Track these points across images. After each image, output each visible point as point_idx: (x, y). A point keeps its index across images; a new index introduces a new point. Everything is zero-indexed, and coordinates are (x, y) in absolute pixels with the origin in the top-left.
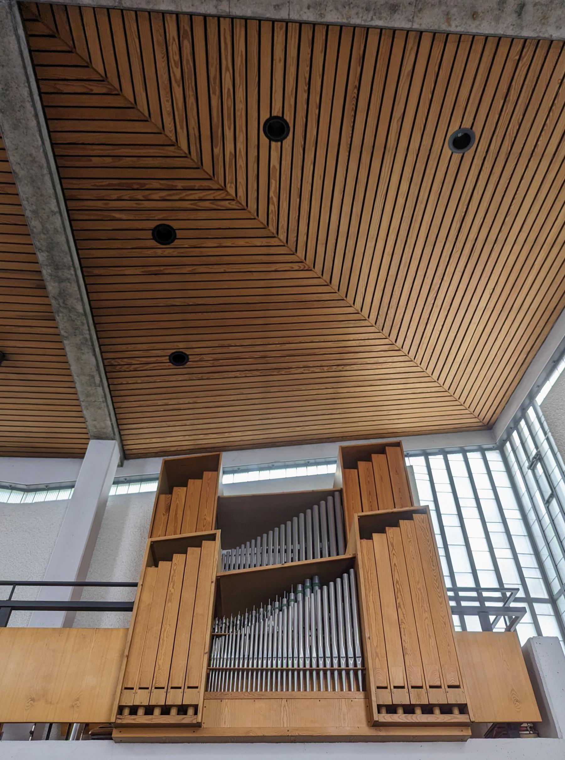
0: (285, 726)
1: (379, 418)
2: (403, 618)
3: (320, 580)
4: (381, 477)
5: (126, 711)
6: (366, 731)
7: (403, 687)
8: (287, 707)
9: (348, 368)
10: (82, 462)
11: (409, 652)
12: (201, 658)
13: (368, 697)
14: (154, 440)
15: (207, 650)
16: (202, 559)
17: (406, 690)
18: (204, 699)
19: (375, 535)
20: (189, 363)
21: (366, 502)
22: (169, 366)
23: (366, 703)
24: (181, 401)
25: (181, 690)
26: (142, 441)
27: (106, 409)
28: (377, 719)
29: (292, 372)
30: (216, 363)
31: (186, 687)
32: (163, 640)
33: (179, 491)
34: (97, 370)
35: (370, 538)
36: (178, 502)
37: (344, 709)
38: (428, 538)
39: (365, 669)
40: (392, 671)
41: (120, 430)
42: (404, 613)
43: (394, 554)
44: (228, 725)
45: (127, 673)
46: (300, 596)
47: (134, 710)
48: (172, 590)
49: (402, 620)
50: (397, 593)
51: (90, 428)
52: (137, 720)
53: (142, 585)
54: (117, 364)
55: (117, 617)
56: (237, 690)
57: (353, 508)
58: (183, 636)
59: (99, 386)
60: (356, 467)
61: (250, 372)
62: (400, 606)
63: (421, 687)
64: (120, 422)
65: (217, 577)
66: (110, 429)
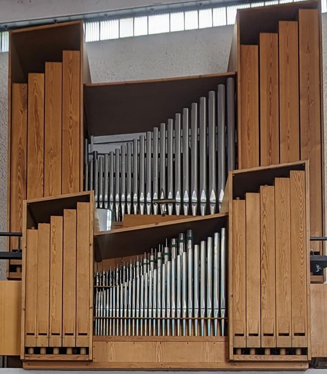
2: (264, 278)
3: (193, 234)
4: (288, 57)
5: (31, 351)
6: (224, 365)
8: (160, 348)
10: (7, 280)
11: (266, 307)
12: (87, 312)
13: (227, 341)
15: (91, 305)
17: (259, 337)
18: (93, 341)
19: (249, 195)
23: (225, 344)
25: (74, 336)
28: (232, 359)
31: (77, 334)
32: (53, 296)
33: (36, 79)
35: (243, 198)
36: (36, 94)
37: (208, 349)
39: (228, 319)
42: (267, 273)
43: (265, 215)
44: (113, 360)
45: (26, 322)
46: (174, 249)
47: (37, 350)
48: (55, 252)
49: (263, 280)
50: (263, 254)
52: (41, 358)
53: (26, 247)
56: (119, 334)
57: (249, 102)
62: (263, 267)
63: (272, 335)
65: (94, 236)
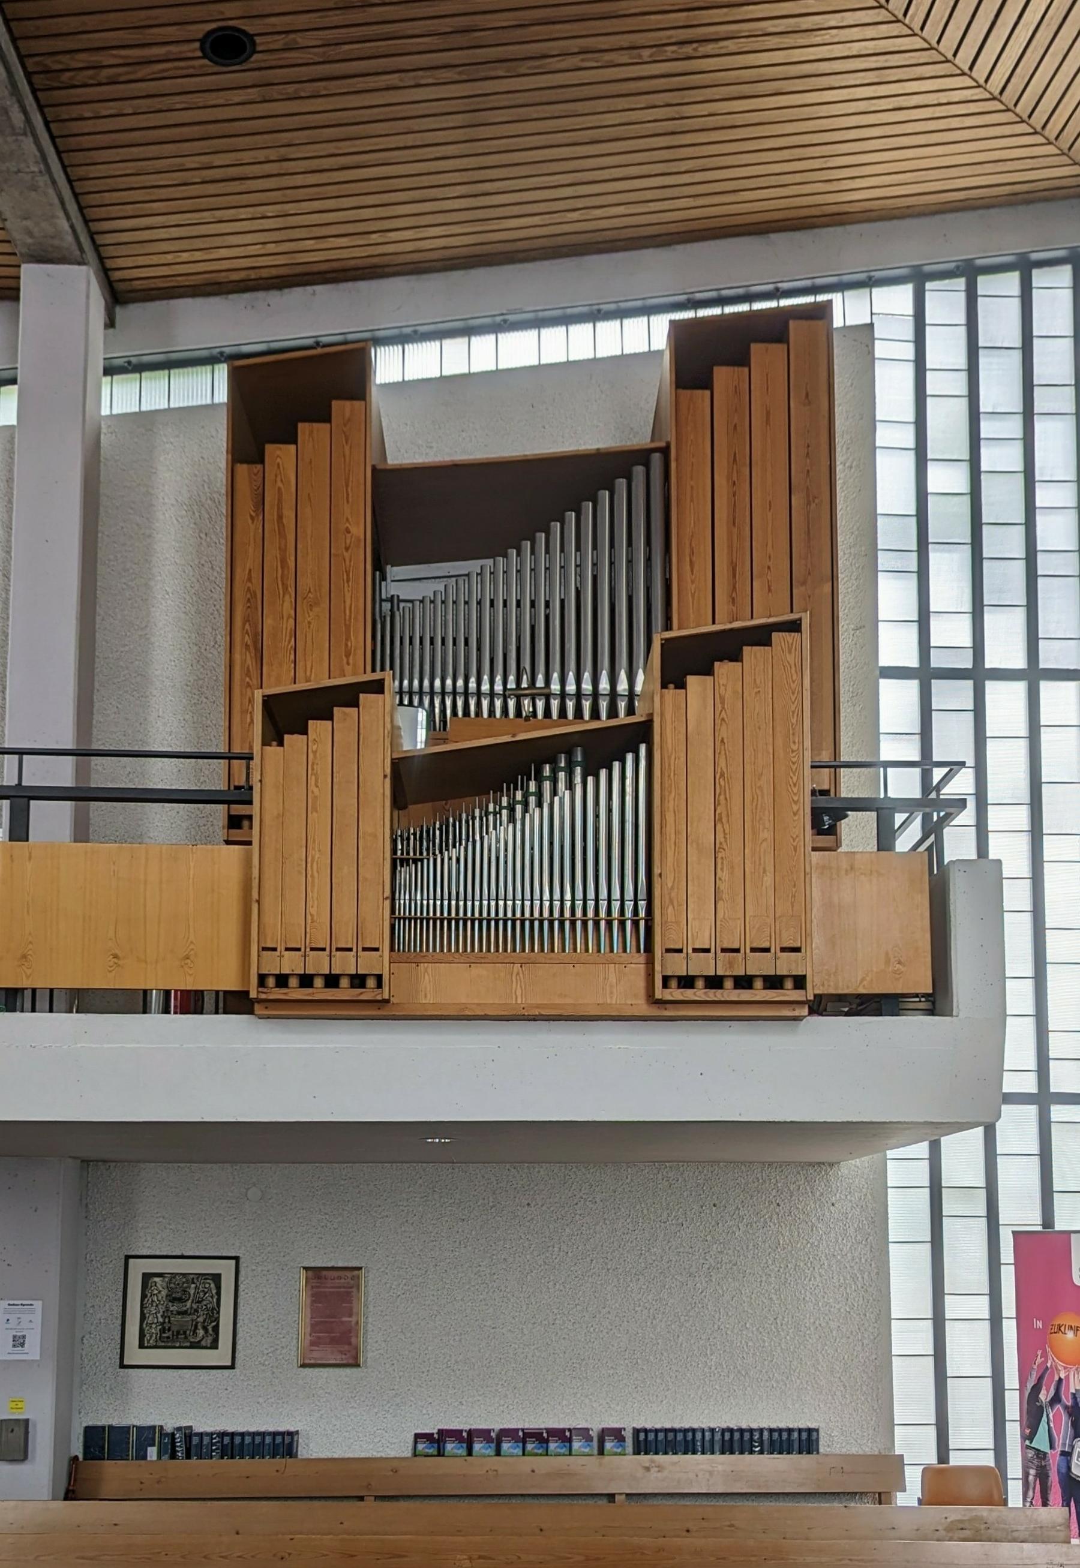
0: (519, 1001)
1: (798, 178)
2: (723, 840)
3: (585, 755)
4: (768, 413)
6: (644, 1009)
7: (708, 951)
9: (710, 48)
13: (650, 963)
14: (185, 257)
15: (388, 893)
16: (361, 731)
19: (692, 680)
20: (255, 57)
21: (724, 482)
22: (202, 66)
23: (647, 969)
24: (247, 157)
26: (155, 260)
27: (51, 191)
29: (553, 68)
30: (332, 52)
31: (360, 949)
32: (312, 876)
33: (280, 455)
34: (12, 94)
35: (681, 685)
36: (279, 484)
37: (613, 978)
38: (793, 686)
40: (695, 924)
41: (92, 235)
42: (727, 831)
43: (723, 719)
44: (430, 999)
46: (547, 785)
47: (282, 980)
48: (316, 790)
51: (17, 235)
53: (261, 781)
54: (60, 67)
55: (179, 717)
58: (346, 871)
59: (25, 134)
60: (706, 383)
61: (428, 73)
62: (721, 819)
63: (737, 951)
64: (91, 213)
65: (392, 759)
66: (70, 238)
